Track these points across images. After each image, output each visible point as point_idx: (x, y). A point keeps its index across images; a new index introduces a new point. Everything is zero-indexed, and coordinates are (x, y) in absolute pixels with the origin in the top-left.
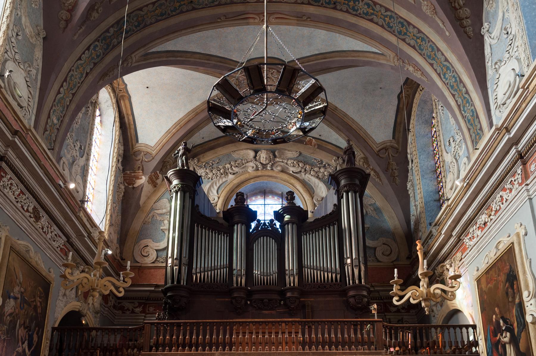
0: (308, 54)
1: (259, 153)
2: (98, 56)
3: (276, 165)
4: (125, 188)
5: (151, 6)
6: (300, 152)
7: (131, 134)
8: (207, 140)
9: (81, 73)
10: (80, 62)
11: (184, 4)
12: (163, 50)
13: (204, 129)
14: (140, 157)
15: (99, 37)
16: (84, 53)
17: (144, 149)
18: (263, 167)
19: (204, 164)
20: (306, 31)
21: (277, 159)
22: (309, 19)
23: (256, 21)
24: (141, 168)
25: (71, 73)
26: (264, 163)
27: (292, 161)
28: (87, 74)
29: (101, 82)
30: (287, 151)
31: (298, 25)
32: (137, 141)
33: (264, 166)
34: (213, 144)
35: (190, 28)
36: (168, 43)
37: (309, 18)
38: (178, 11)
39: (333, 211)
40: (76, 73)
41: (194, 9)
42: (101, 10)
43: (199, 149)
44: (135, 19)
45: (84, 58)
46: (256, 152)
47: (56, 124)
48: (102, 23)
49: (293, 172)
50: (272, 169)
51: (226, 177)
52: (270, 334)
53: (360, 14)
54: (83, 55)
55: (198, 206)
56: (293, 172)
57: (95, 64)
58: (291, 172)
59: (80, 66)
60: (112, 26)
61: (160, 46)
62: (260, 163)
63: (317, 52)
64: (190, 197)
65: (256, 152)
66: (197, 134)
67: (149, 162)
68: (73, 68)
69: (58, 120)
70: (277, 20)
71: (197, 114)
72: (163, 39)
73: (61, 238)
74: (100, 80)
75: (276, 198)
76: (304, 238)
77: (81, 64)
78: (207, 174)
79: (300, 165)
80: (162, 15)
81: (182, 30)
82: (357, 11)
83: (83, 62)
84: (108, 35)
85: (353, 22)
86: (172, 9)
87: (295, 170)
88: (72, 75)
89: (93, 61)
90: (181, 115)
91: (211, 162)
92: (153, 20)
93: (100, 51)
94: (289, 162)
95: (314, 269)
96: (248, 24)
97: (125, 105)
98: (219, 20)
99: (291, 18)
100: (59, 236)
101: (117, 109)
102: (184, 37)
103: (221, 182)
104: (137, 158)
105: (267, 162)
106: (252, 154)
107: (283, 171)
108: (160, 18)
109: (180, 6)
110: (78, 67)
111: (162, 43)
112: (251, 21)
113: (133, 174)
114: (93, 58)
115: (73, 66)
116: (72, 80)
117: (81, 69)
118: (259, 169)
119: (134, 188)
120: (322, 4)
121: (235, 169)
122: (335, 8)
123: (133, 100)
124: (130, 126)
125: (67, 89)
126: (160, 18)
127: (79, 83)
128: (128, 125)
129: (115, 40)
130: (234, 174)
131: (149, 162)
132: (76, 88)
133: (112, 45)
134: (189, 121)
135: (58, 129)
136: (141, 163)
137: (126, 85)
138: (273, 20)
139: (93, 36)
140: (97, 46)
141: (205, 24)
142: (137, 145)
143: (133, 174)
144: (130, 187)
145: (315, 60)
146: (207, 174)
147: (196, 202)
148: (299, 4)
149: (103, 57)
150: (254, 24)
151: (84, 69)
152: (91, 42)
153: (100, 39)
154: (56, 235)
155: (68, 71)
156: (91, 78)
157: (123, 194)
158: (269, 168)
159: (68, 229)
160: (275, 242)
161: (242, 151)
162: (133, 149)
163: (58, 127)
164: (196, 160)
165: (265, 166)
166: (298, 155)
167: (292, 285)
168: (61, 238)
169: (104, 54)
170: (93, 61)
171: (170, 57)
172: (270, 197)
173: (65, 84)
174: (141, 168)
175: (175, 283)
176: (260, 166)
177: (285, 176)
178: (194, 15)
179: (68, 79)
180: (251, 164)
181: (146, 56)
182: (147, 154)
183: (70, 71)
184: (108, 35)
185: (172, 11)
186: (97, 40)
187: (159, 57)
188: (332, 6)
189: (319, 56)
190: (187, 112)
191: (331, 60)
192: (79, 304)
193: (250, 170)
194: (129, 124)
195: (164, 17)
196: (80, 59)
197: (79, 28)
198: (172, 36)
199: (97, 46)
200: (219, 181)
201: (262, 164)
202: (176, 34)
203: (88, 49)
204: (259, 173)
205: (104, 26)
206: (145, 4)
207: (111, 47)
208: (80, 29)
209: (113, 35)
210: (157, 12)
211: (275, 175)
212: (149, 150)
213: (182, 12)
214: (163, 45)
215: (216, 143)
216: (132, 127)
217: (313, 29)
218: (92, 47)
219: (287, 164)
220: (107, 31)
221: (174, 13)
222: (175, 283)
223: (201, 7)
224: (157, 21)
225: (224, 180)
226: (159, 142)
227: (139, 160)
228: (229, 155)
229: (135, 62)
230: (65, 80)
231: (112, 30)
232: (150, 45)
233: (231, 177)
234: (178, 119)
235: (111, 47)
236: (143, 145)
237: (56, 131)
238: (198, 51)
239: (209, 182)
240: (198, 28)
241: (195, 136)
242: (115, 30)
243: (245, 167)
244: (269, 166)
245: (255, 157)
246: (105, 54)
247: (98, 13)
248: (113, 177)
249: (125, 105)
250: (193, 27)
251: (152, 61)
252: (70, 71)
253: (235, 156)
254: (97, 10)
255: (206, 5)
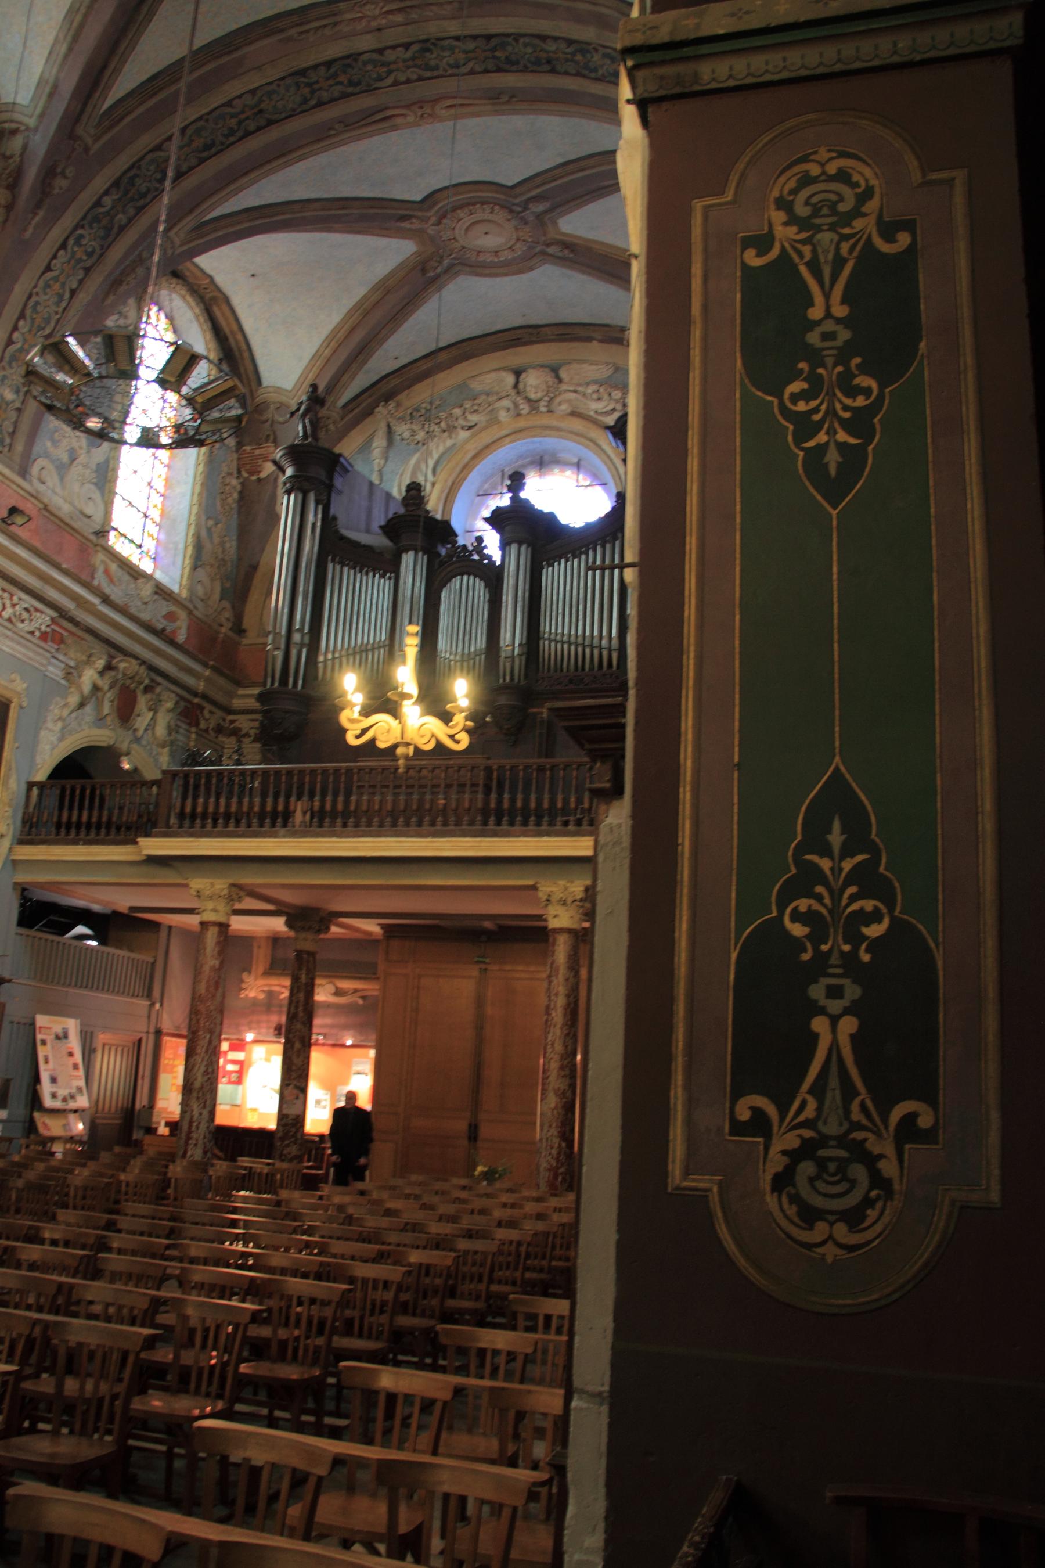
0: (547, 166)
1: (523, 376)
2: (90, 255)
3: (557, 400)
4: (242, 484)
5: (323, 69)
6: (614, 364)
7: (246, 370)
8: (404, 361)
9: (58, 294)
10: (49, 275)
11: (247, 118)
12: (236, 209)
13: (391, 342)
14: (268, 415)
15: (83, 218)
16: (55, 257)
17: (273, 397)
18: (531, 406)
19: (409, 411)
20: (518, 122)
21: (564, 387)
22: (515, 99)
23: (411, 119)
24: (272, 438)
25: (34, 299)
26: (533, 396)
27: (595, 387)
28: (73, 293)
29: (111, 298)
30: (585, 366)
31: (498, 113)
32: (259, 382)
33: (533, 403)
34: (424, 367)
35: (278, 157)
36: (242, 194)
37: (513, 96)
38: (239, 134)
39: (613, 508)
40: (46, 297)
41: (270, 123)
42: (70, 172)
43: (395, 381)
44: (152, 168)
45: (59, 266)
46: (518, 373)
47: (13, 401)
48: (80, 192)
49: (596, 412)
50: (550, 411)
51: (453, 436)
52: (410, 790)
53: (603, 75)
54: (55, 261)
55: (335, 518)
56: (596, 412)
57: (87, 270)
58: (592, 413)
59: (51, 282)
60: (107, 193)
61: (226, 204)
62: (526, 398)
63: (561, 160)
64: (317, 502)
65: (518, 373)
66: (380, 352)
67: (286, 422)
68: (35, 290)
69: (17, 392)
70: (453, 111)
71: (366, 314)
72: (224, 193)
73: (42, 612)
74: (107, 294)
75: (568, 473)
76: (547, 573)
77: (56, 279)
78: (413, 433)
79: (613, 394)
80: (207, 147)
81: (262, 165)
82: (596, 70)
83: (56, 273)
84: (102, 210)
85: (601, 93)
86: (226, 132)
87: (599, 406)
88: (37, 303)
89: (82, 265)
90: (336, 318)
91: (424, 405)
92: (194, 161)
93: (93, 243)
94: (590, 390)
95: (557, 642)
96: (395, 128)
97: (223, 314)
98: (332, 132)
99: (471, 102)
100: (37, 610)
101: (209, 325)
102: (273, 177)
103: (441, 449)
104: (264, 418)
105: (539, 395)
106: (510, 379)
107: (574, 414)
108: (205, 154)
109: (240, 123)
110: (47, 286)
111: (226, 199)
112: (399, 121)
113: (257, 452)
114: (80, 261)
115: (35, 287)
116: (37, 313)
117: (57, 286)
118: (523, 412)
119: (259, 480)
120: (526, 67)
121: (473, 418)
122: (553, 71)
123: (236, 301)
124: (241, 354)
125: (30, 331)
126: (205, 154)
127: (57, 313)
128: (237, 353)
129: (120, 216)
130: (470, 428)
131: (286, 422)
132: (53, 324)
133: (116, 226)
134: (353, 329)
135: (19, 410)
136: (272, 425)
137: (211, 278)
138: (443, 111)
139: (68, 220)
140: (82, 236)
141: (307, 145)
142: (261, 391)
143: (257, 452)
144: (254, 478)
145: (544, 184)
146: (413, 433)
147: (332, 512)
148: (479, 73)
149: (102, 255)
150: (409, 125)
151: (63, 285)
152: (66, 234)
153: (85, 222)
154: (26, 609)
155: (25, 298)
156: (83, 298)
157: (236, 495)
158: (543, 409)
159: (53, 594)
160: (486, 587)
161: (488, 376)
162: (253, 398)
163: (18, 405)
164: (392, 405)
165: (536, 405)
166: (611, 372)
167: (516, 680)
168: (42, 612)
169: (102, 247)
170: (82, 265)
171: (258, 218)
172: (556, 471)
173: (21, 323)
174: (272, 438)
175: (276, 685)
176: (525, 408)
177: (577, 425)
178: (274, 134)
179: (28, 312)
180: (506, 403)
181: (200, 228)
182: (280, 406)
183: (30, 297)
184: (102, 210)
185: (226, 136)
186: (79, 226)
187: (215, 230)
188: (547, 67)
189: (571, 167)
190: (344, 311)
191: (594, 171)
192: (106, 732)
193: (503, 416)
194: (239, 349)
195: (214, 150)
196: (48, 269)
197: (30, 216)
198: (245, 179)
199: (82, 236)
200: (437, 447)
201: (529, 400)
202: (252, 175)
203: (63, 246)
204: (522, 423)
205: (86, 198)
206: (164, 137)
207: (115, 230)
208: (32, 218)
209: (113, 208)
210: (194, 145)
211: (555, 423)
212: (284, 399)
213: (248, 134)
214: (232, 201)
215: (429, 365)
216: (246, 355)
217: (531, 117)
218: (71, 241)
219: (584, 395)
220: (98, 203)
221: (232, 139)
222: (276, 685)
223: (283, 115)
224: (202, 161)
225: (449, 443)
226: (301, 380)
227: (267, 421)
228: (463, 386)
229: (181, 246)
230: (22, 316)
231: (108, 201)
232: (204, 206)
233: (463, 435)
234: (331, 327)
235: (115, 230)
236: (271, 390)
237: (13, 415)
238: (313, 196)
239: (416, 451)
240: (295, 155)
241: (374, 357)
242: (116, 197)
243: (492, 410)
244: (542, 403)
245: (516, 386)
246: (105, 248)
247: (66, 178)
248: (202, 466)
249: (223, 314)
250: (283, 155)
251: (220, 233)
252: (30, 297)
253: (476, 386)
254: (63, 174)
255: (294, 110)
